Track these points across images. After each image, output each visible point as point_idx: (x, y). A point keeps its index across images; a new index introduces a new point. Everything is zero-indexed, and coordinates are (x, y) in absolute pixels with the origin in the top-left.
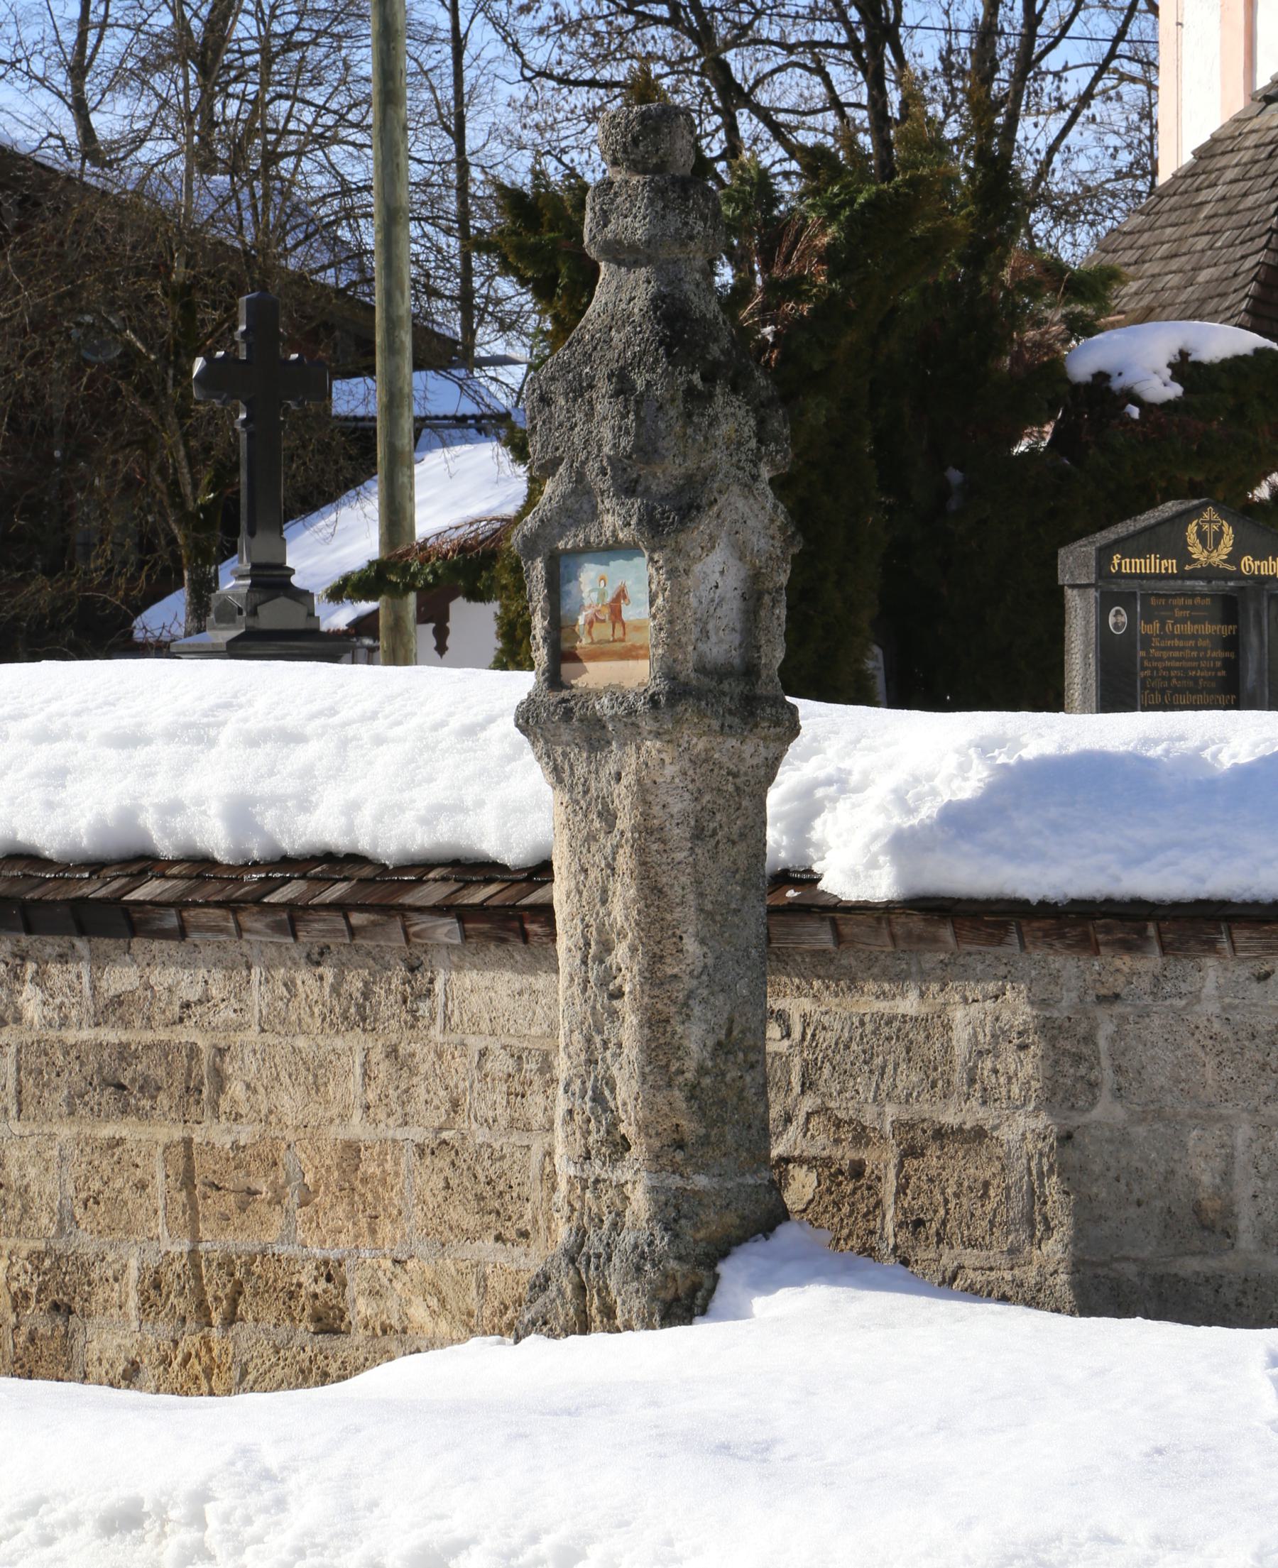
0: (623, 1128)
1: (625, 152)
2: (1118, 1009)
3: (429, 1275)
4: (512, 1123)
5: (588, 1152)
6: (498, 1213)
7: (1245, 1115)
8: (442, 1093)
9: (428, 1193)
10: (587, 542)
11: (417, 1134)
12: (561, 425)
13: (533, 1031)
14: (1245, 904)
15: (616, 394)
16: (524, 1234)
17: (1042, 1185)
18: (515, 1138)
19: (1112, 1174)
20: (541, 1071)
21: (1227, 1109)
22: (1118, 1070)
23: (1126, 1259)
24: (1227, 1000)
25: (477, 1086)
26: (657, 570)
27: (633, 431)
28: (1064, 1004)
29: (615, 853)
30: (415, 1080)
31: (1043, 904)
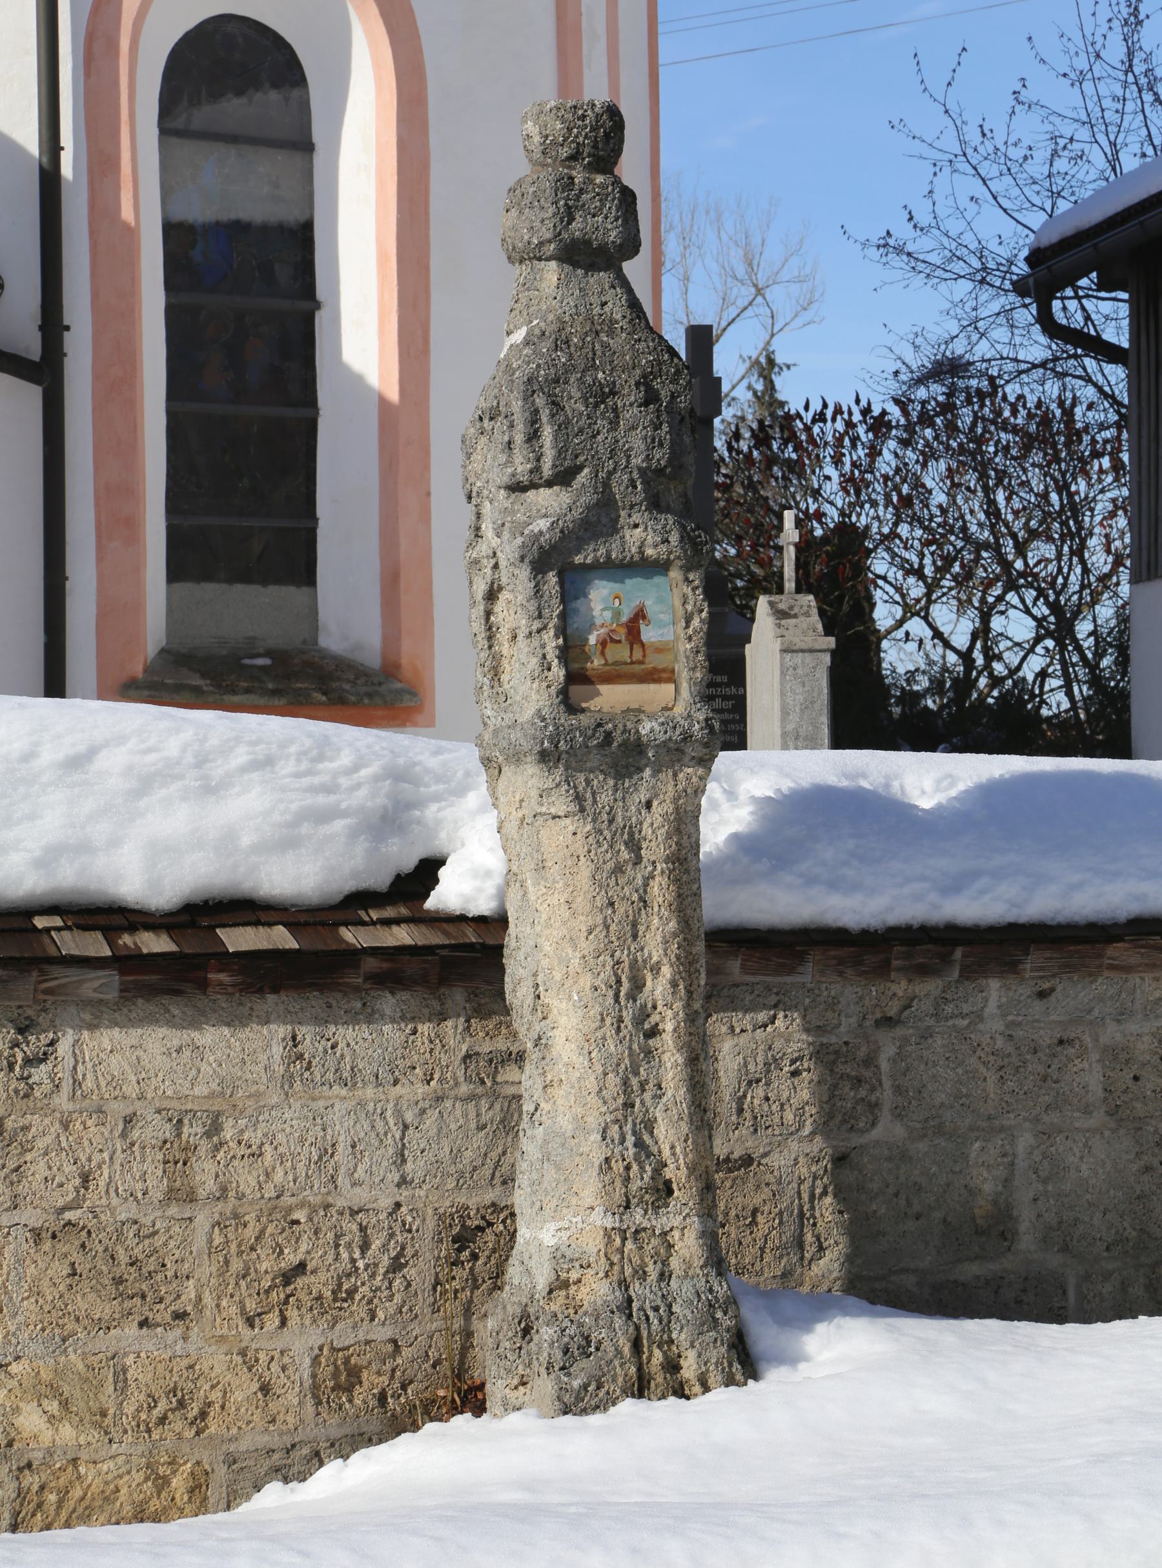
0: (668, 1173)
1: (595, 147)
2: (899, 1032)
3: (45, 1376)
4: (171, 1195)
5: (628, 1202)
6: (144, 1297)
7: (1027, 1125)
8: (68, 1168)
9: (46, 1283)
10: (608, 556)
11: (31, 1217)
12: (581, 431)
13: (197, 1091)
14: (1060, 926)
15: (646, 403)
16: (180, 1316)
17: (812, 1208)
18: (173, 1210)
19: (891, 1190)
20: (208, 1135)
21: (1010, 1120)
22: (898, 1090)
23: (906, 1271)
24: (1010, 1018)
25: (120, 1156)
26: (694, 589)
27: (667, 444)
28: (842, 1029)
29: (646, 885)
30: (29, 1157)
31: (865, 932)
